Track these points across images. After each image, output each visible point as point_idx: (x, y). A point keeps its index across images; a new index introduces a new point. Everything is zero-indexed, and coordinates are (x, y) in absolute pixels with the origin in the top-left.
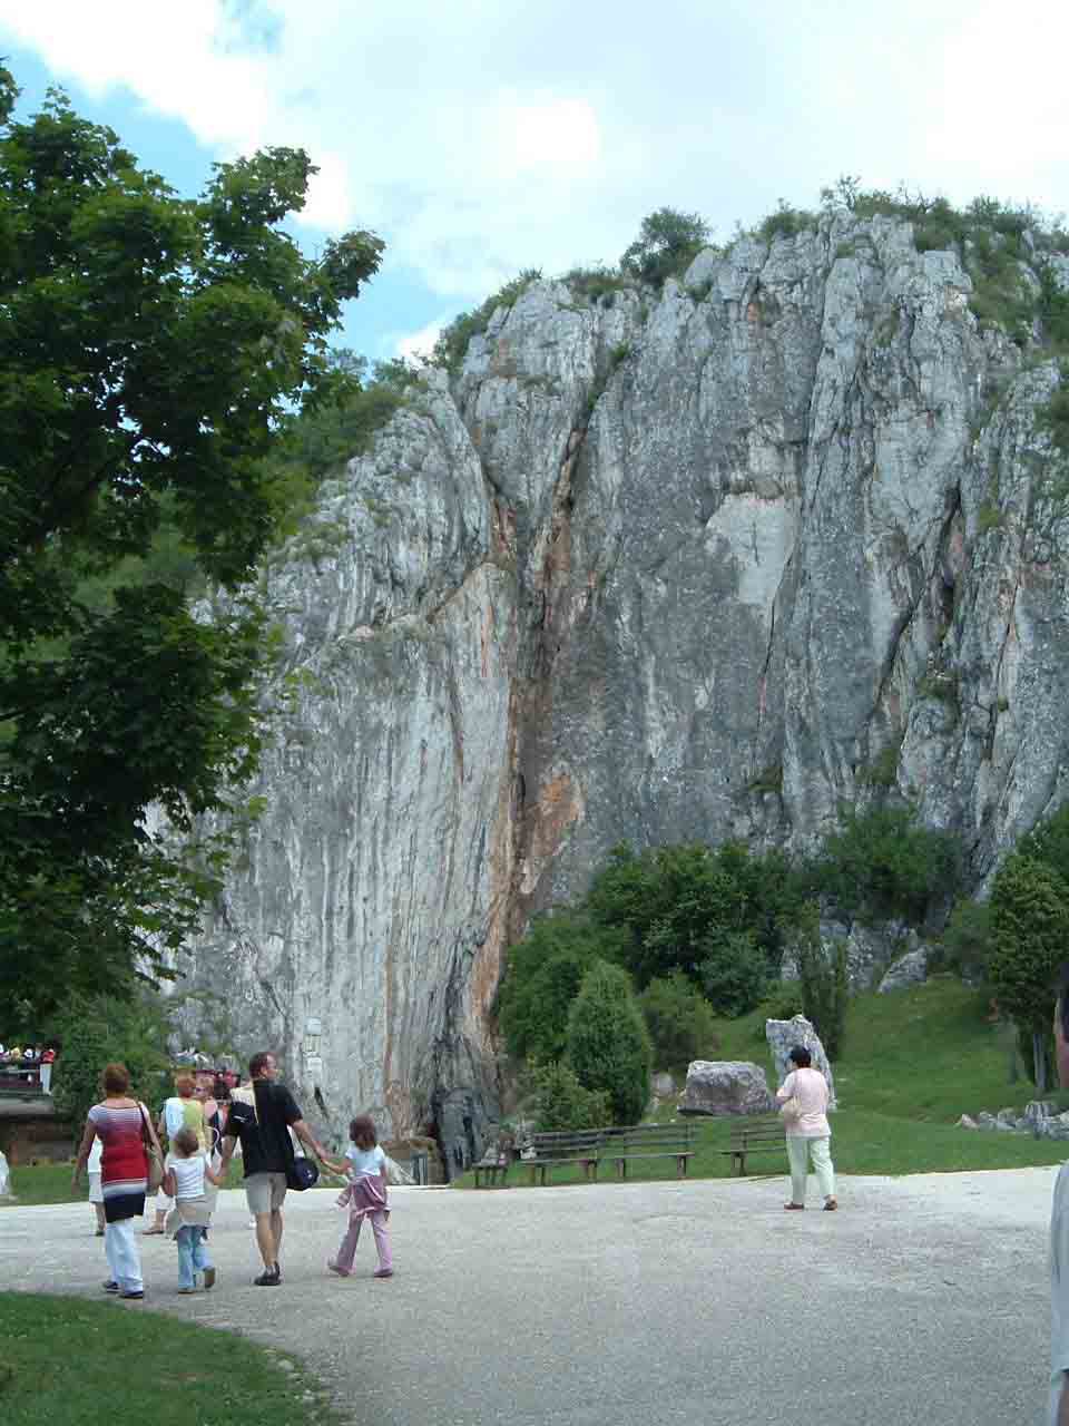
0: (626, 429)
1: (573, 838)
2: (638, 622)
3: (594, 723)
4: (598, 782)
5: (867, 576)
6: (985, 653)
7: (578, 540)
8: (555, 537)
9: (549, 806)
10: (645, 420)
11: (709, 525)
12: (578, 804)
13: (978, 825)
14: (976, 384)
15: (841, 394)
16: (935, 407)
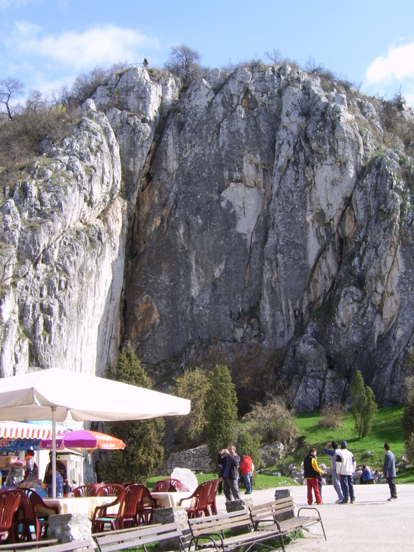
0: (181, 144)
1: (153, 331)
2: (187, 234)
3: (164, 279)
4: (166, 307)
5: (307, 229)
6: (383, 271)
7: (156, 192)
8: (143, 190)
9: (140, 315)
10: (190, 142)
11: (222, 194)
12: (155, 316)
13: (375, 342)
14: (360, 155)
15: (292, 146)
16: (344, 161)
